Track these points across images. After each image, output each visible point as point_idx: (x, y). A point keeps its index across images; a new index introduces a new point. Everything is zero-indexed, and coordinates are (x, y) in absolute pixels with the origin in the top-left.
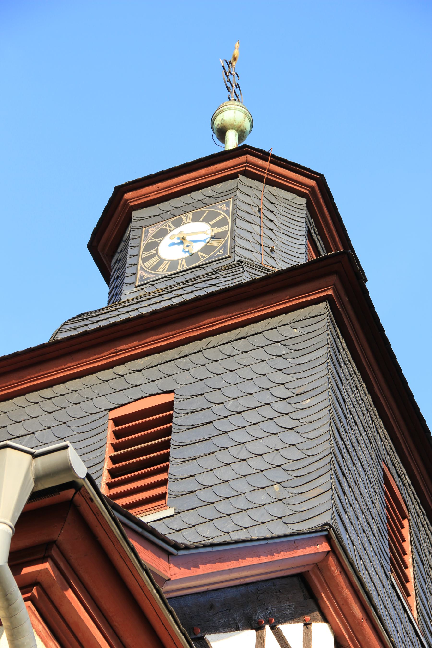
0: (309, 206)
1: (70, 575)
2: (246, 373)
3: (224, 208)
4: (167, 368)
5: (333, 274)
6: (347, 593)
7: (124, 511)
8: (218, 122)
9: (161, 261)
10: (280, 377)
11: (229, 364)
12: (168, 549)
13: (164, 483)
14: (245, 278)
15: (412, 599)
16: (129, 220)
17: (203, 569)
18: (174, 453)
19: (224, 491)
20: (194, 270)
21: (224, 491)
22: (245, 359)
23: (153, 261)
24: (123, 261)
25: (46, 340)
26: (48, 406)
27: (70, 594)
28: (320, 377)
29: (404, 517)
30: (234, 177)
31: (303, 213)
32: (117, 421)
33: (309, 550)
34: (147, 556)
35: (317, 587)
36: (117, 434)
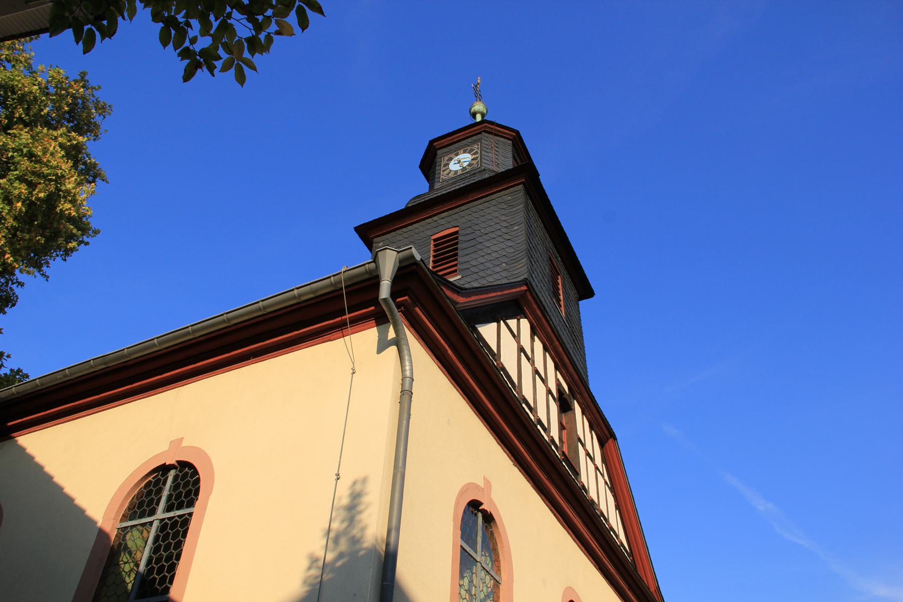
0: (513, 145)
1: (416, 301)
2: (489, 217)
4: (455, 217)
5: (524, 172)
6: (535, 306)
7: (441, 277)
8: (472, 110)
10: (504, 218)
11: (481, 213)
12: (456, 289)
13: (456, 265)
14: (487, 176)
15: (563, 308)
16: (436, 155)
17: (473, 298)
18: (460, 252)
19: (481, 267)
20: (465, 173)
21: (481, 267)
22: (488, 211)
24: (434, 172)
26: (406, 235)
27: (417, 309)
28: (521, 217)
30: (480, 133)
31: (510, 148)
32: (435, 240)
33: (518, 289)
34: (449, 293)
36: (435, 246)
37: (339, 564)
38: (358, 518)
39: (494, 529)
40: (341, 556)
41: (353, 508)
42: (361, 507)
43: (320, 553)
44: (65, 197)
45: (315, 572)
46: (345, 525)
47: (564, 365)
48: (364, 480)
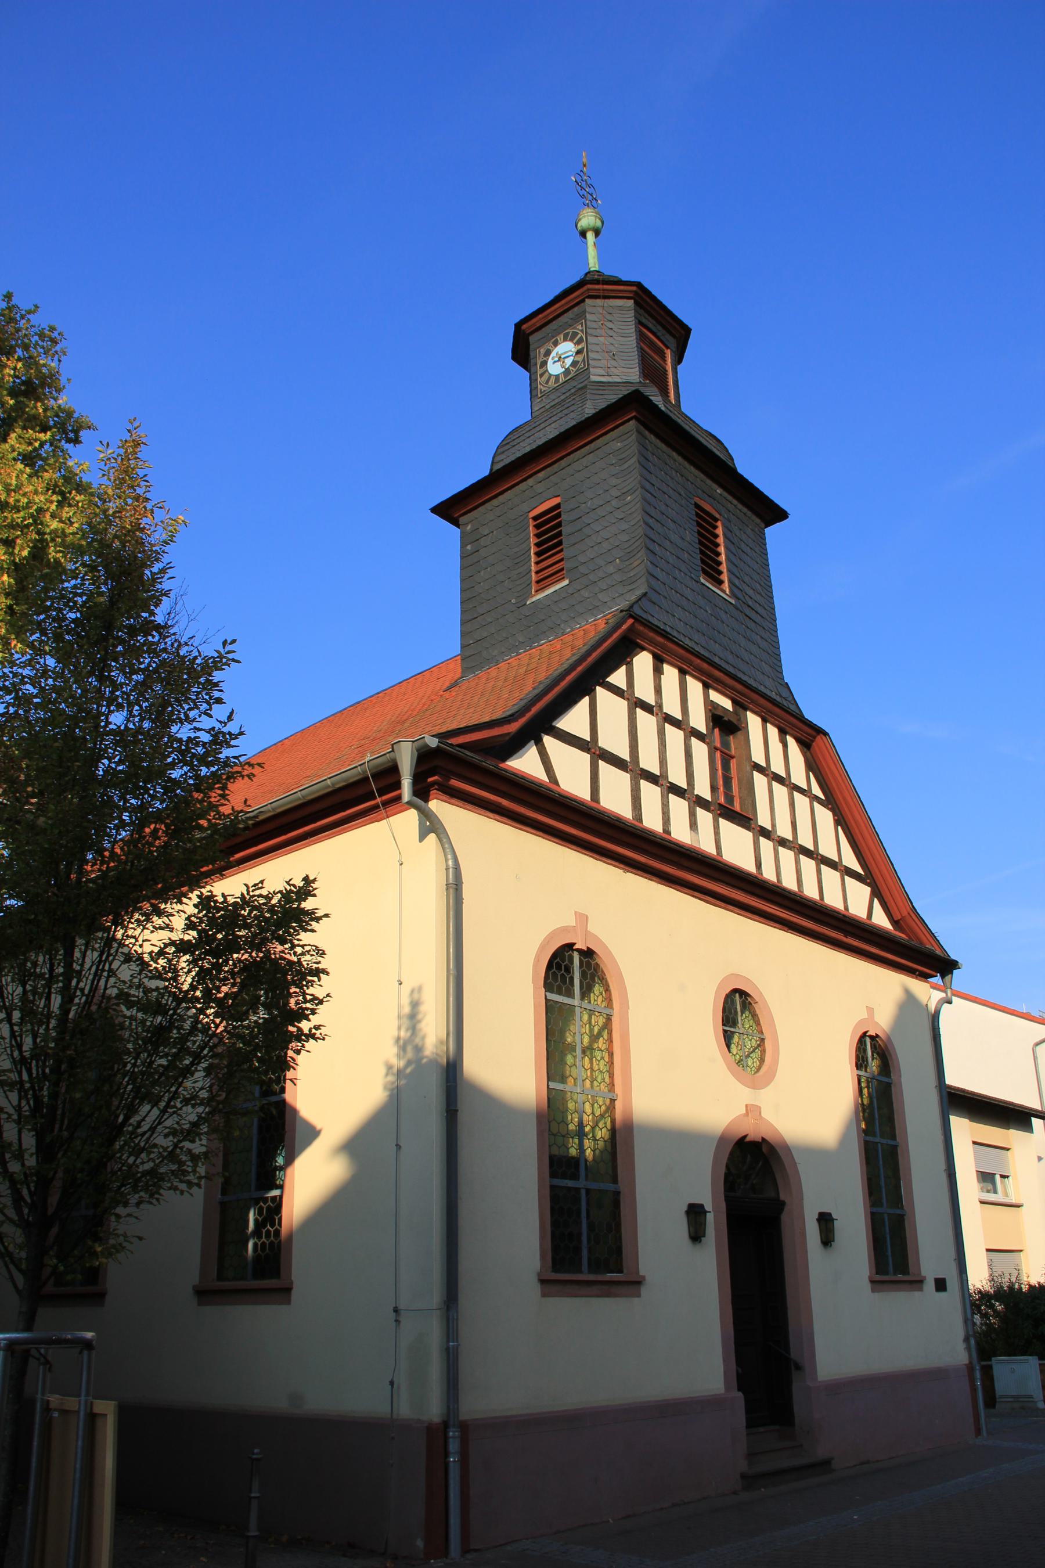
0: (636, 302)
1: (447, 775)
3: (580, 327)
4: (553, 478)
9: (550, 375)
23: (546, 376)
25: (486, 473)
29: (716, 520)
32: (535, 518)
35: (105, 1458)
36: (537, 527)
37: (408, 1070)
38: (419, 1026)
39: (598, 961)
40: (409, 1063)
41: (413, 1018)
42: (420, 1016)
43: (394, 1061)
44: (53, 540)
45: (391, 1078)
46: (409, 1034)
47: (718, 681)
48: (420, 989)
